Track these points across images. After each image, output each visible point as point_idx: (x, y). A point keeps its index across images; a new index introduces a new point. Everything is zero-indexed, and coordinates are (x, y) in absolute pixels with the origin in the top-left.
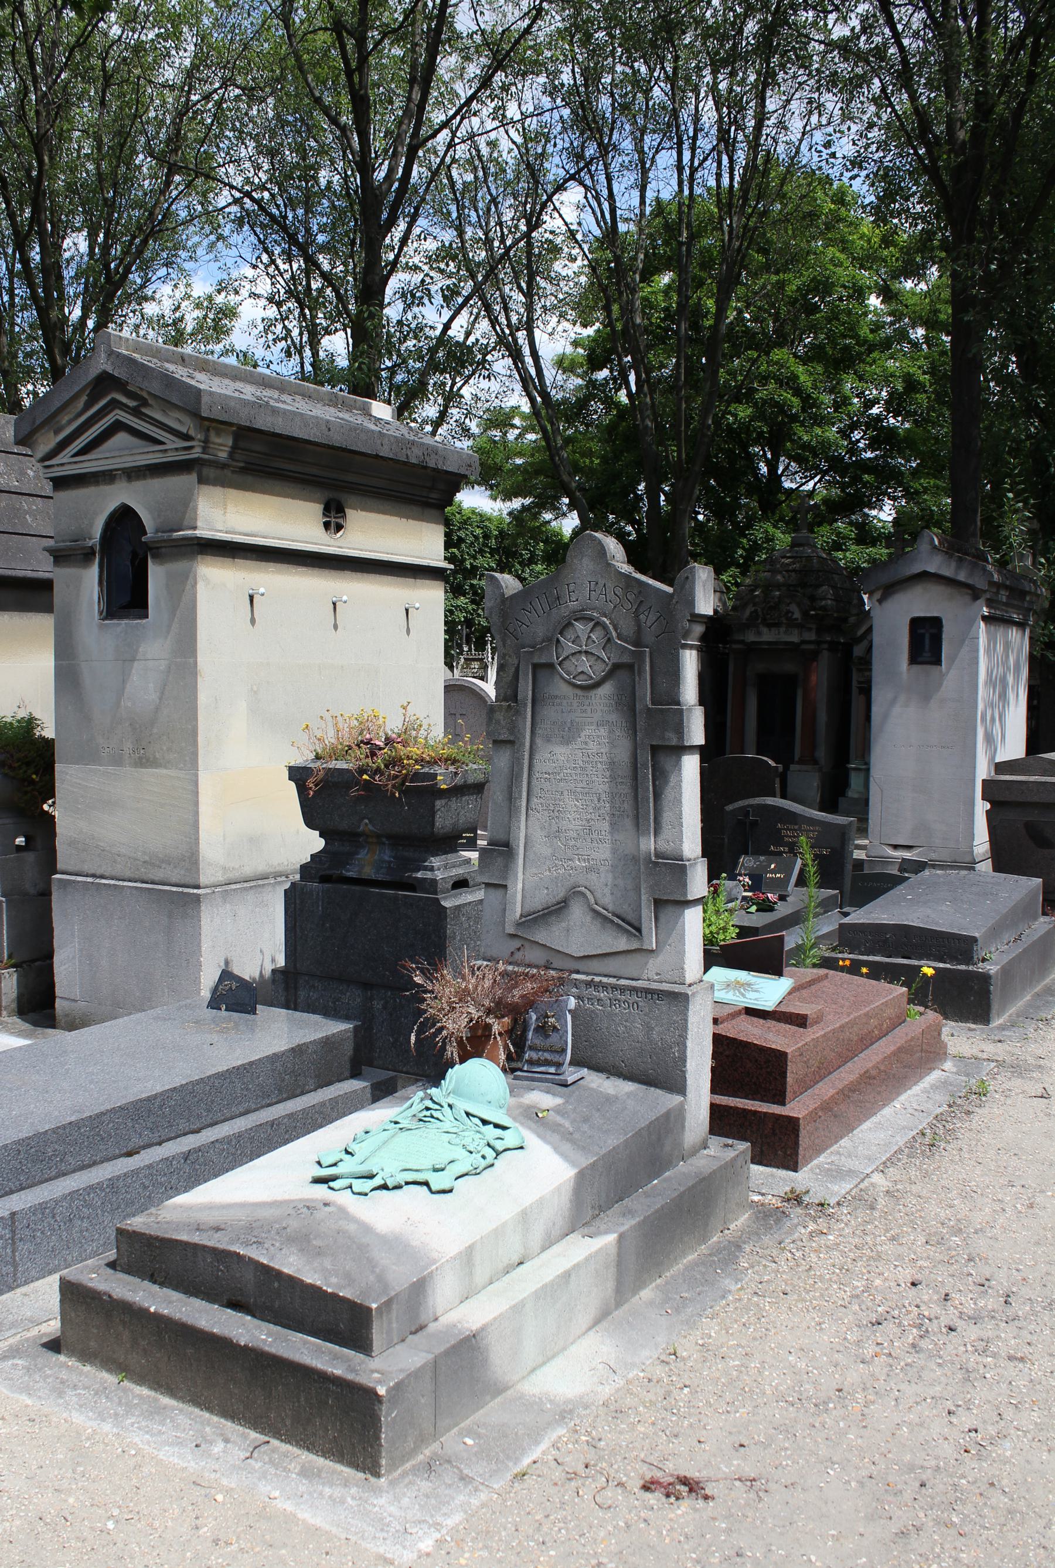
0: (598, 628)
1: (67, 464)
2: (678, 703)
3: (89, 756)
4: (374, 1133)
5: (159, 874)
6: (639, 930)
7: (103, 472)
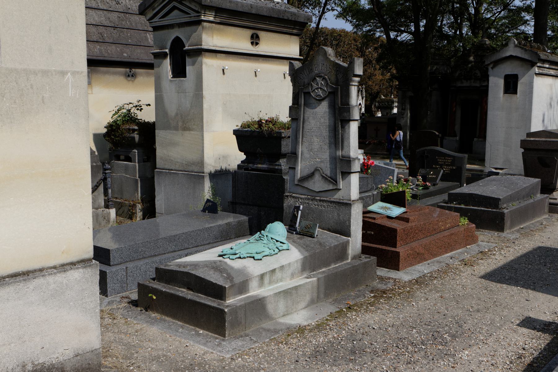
2: (349, 105)
3: (167, 127)
4: (242, 245)
5: (190, 169)
6: (336, 182)
7: (170, 25)
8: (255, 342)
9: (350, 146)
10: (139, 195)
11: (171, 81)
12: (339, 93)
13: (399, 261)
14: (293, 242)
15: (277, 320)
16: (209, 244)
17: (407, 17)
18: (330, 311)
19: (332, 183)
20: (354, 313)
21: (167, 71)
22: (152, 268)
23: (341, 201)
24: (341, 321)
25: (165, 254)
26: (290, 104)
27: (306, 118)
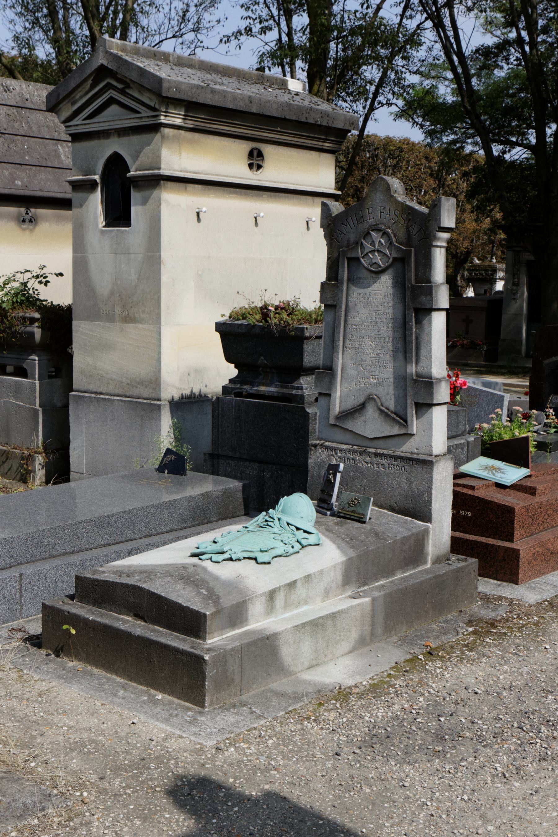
0: (385, 236)
1: (80, 124)
2: (430, 282)
3: (94, 315)
4: (236, 536)
6: (406, 421)
8: (259, 717)
9: (431, 357)
10: (41, 438)
11: (102, 232)
12: (413, 260)
13: (518, 566)
14: (327, 530)
15: (298, 675)
16: (171, 531)
17: (520, 118)
18: (395, 659)
19: (398, 422)
20: (439, 664)
21: (95, 213)
22: (68, 575)
23: (415, 456)
24: (415, 677)
25: (90, 549)
26: (323, 277)
27: (351, 304)
